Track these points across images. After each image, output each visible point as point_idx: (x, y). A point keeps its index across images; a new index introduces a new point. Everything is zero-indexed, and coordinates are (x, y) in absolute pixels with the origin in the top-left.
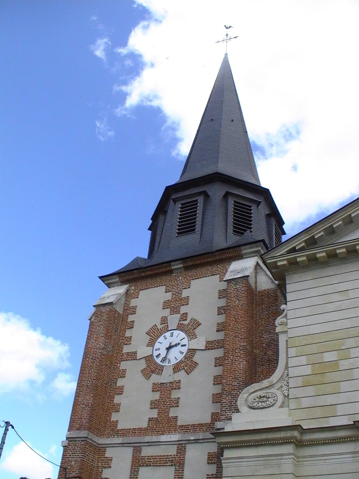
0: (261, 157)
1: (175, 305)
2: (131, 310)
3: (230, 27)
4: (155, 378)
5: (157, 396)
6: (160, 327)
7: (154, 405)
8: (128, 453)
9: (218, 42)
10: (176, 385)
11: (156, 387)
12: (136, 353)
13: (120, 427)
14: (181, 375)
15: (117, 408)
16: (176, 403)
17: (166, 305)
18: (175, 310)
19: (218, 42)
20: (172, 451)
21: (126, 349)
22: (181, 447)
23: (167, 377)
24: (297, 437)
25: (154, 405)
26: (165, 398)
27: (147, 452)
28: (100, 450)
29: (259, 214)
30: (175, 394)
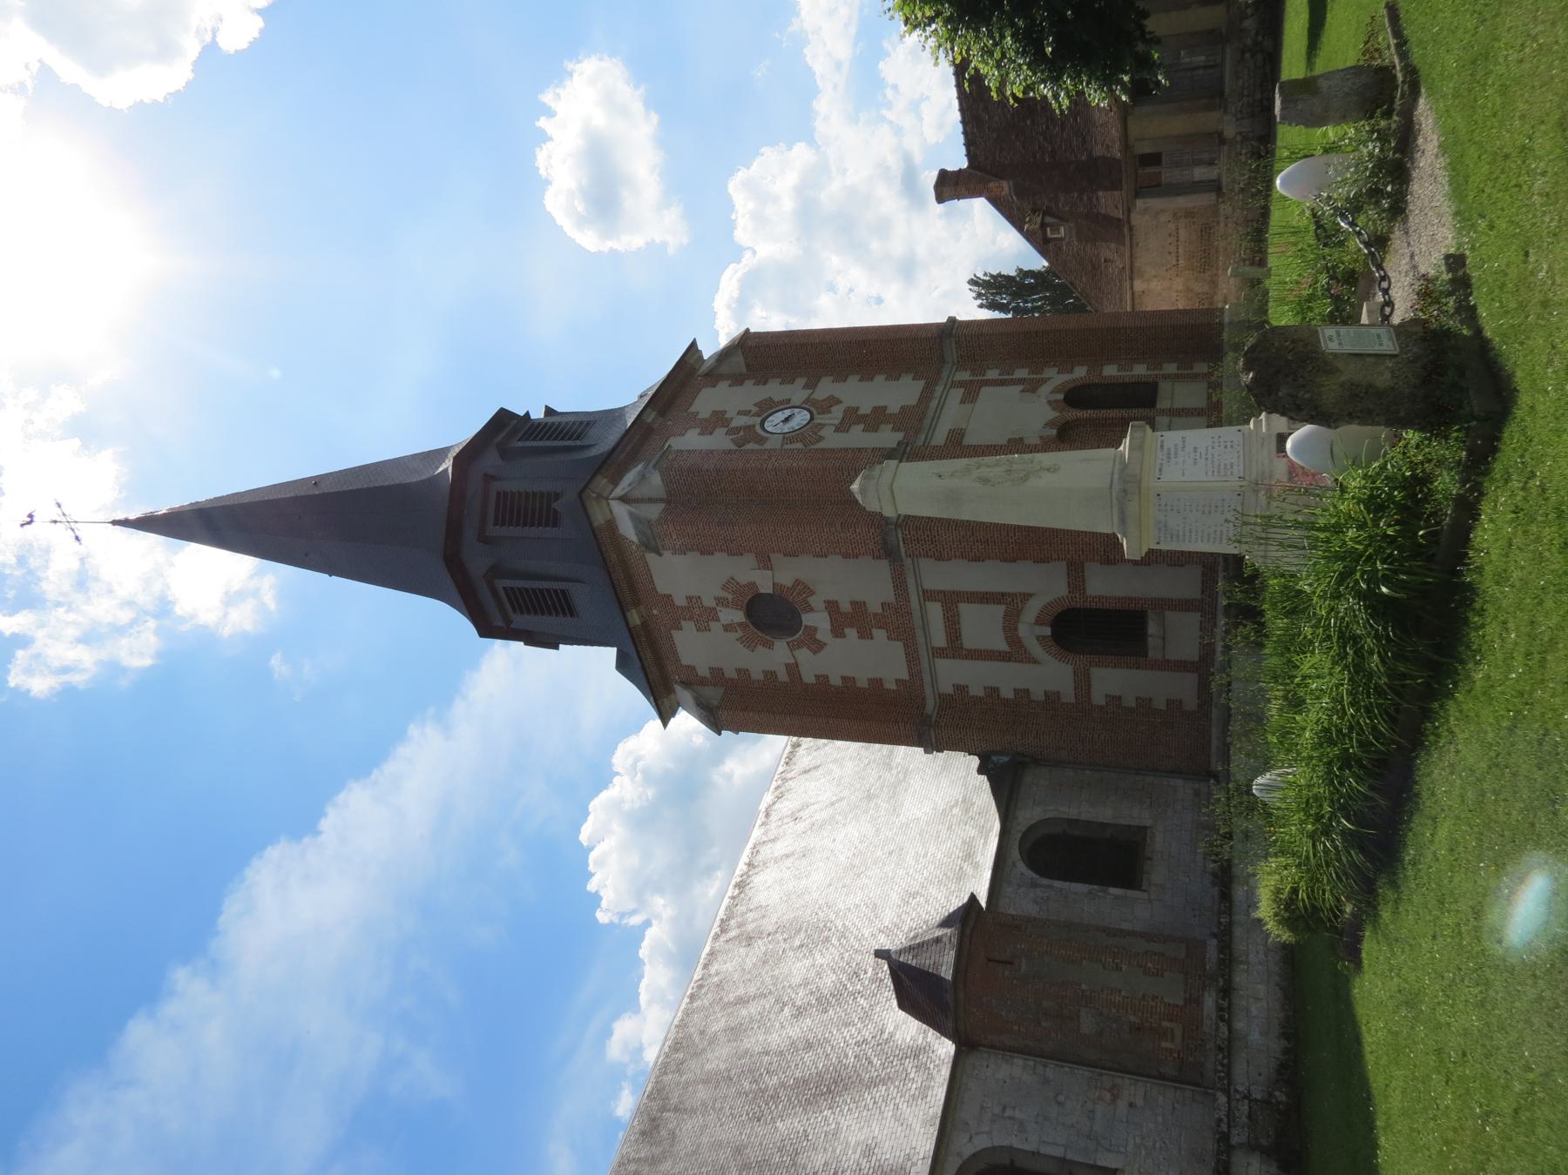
0: (924, 961)
2: (717, 675)
3: (31, 516)
5: (851, 633)
8: (942, 664)
9: (77, 538)
11: (838, 632)
12: (787, 665)
13: (906, 676)
15: (877, 683)
16: (859, 606)
17: (703, 628)
18: (712, 614)
19: (77, 538)
20: (935, 610)
21: (783, 676)
22: (929, 595)
24: (1402, 42)
25: (865, 634)
27: (939, 639)
28: (945, 701)
29: (520, 479)
30: (845, 607)
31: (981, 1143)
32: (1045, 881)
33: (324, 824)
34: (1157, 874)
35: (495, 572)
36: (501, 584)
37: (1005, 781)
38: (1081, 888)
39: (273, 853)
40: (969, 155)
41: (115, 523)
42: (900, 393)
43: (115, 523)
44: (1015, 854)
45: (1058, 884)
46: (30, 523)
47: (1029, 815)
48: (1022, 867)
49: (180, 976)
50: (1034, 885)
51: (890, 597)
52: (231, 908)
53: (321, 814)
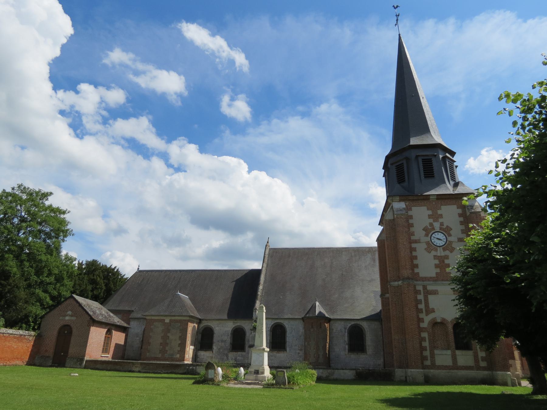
1: (435, 217)
3: (397, 6)
4: (433, 253)
6: (430, 228)
7: (437, 266)
10: (447, 257)
14: (447, 253)
17: (430, 216)
23: (440, 253)
25: (437, 266)
26: (442, 264)
31: (287, 326)
32: (347, 331)
33: (531, 22)
34: (353, 356)
35: (408, 159)
36: (404, 162)
37: (374, 318)
38: (346, 339)
39: (508, 14)
40: (89, 330)
41: (399, 35)
42: (172, 314)
43: (399, 35)
44: (353, 323)
45: (346, 334)
46: (395, 8)
47: (365, 325)
48: (350, 325)
49: (452, 21)
50: (345, 329)
51: (421, 275)
52: (482, 17)
53: (533, 17)
